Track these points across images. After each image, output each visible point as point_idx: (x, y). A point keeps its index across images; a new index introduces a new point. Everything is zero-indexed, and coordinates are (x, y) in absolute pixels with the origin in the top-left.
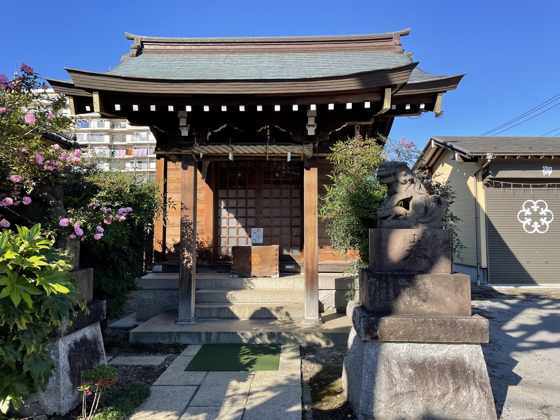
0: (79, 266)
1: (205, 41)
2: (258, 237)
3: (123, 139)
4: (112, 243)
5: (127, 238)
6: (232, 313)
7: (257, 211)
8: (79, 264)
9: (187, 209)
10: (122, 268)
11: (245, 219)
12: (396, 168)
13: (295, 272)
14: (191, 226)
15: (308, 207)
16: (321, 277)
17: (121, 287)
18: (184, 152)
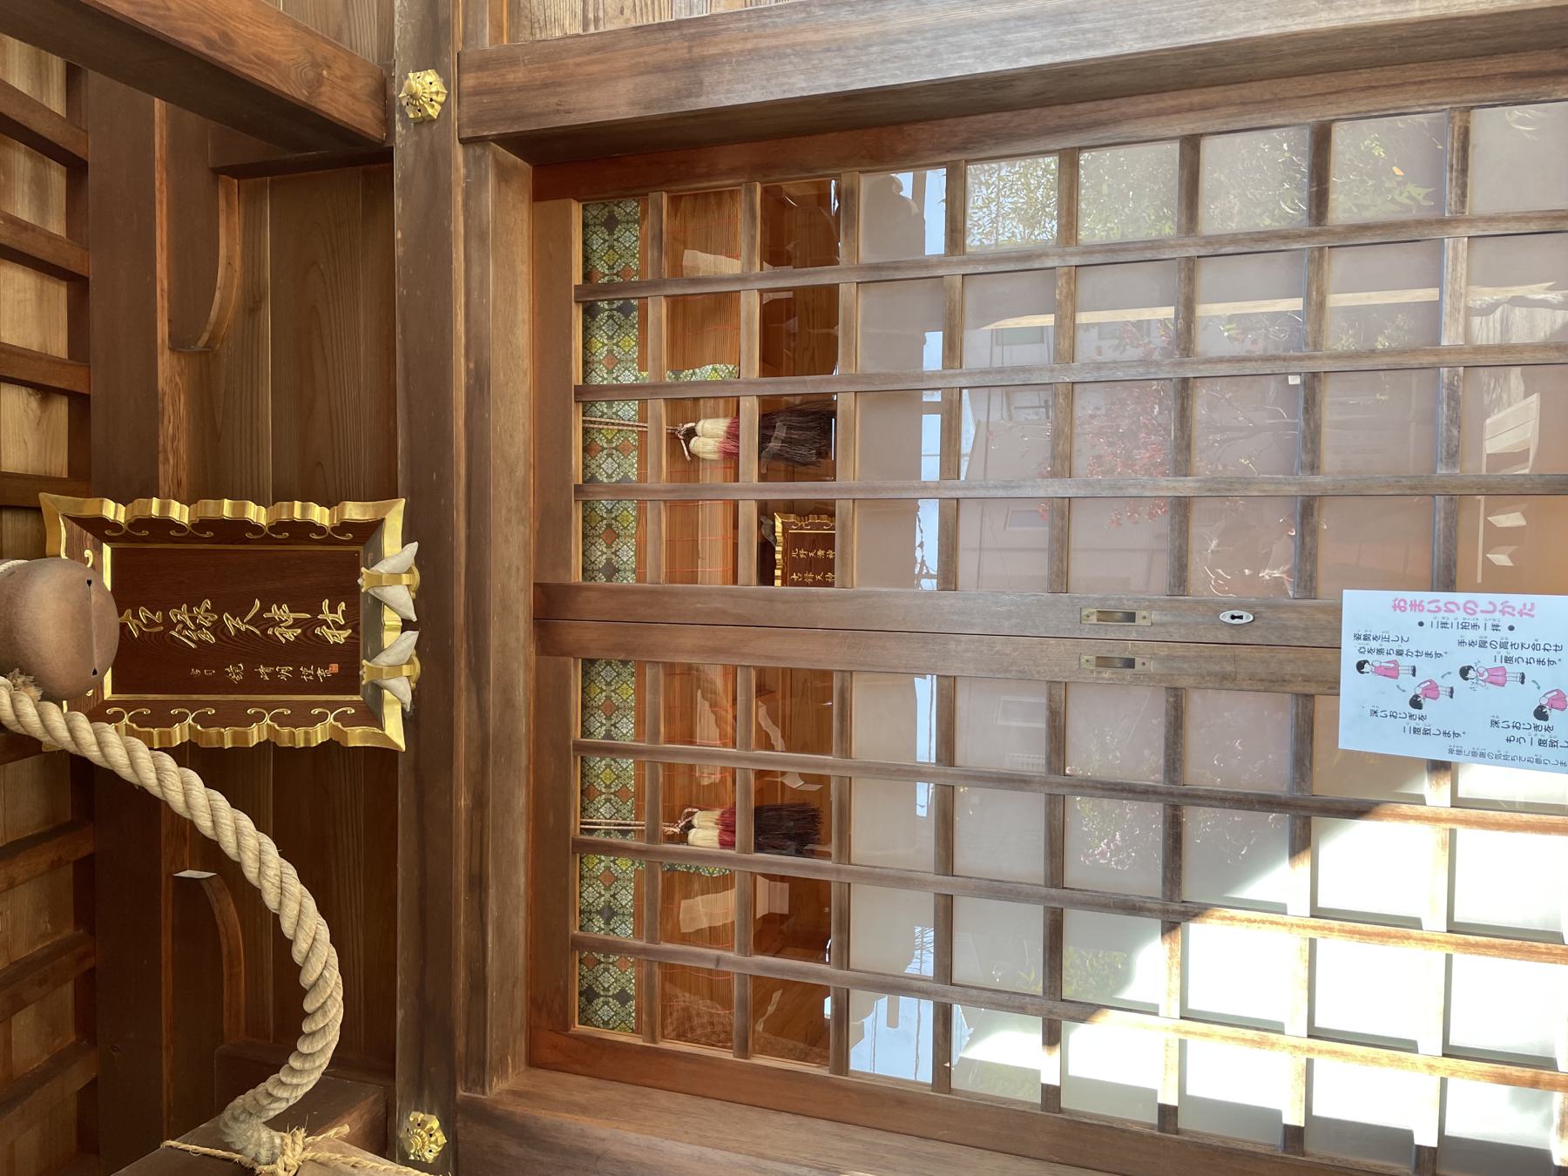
2: (1485, 659)
7: (1103, 662)
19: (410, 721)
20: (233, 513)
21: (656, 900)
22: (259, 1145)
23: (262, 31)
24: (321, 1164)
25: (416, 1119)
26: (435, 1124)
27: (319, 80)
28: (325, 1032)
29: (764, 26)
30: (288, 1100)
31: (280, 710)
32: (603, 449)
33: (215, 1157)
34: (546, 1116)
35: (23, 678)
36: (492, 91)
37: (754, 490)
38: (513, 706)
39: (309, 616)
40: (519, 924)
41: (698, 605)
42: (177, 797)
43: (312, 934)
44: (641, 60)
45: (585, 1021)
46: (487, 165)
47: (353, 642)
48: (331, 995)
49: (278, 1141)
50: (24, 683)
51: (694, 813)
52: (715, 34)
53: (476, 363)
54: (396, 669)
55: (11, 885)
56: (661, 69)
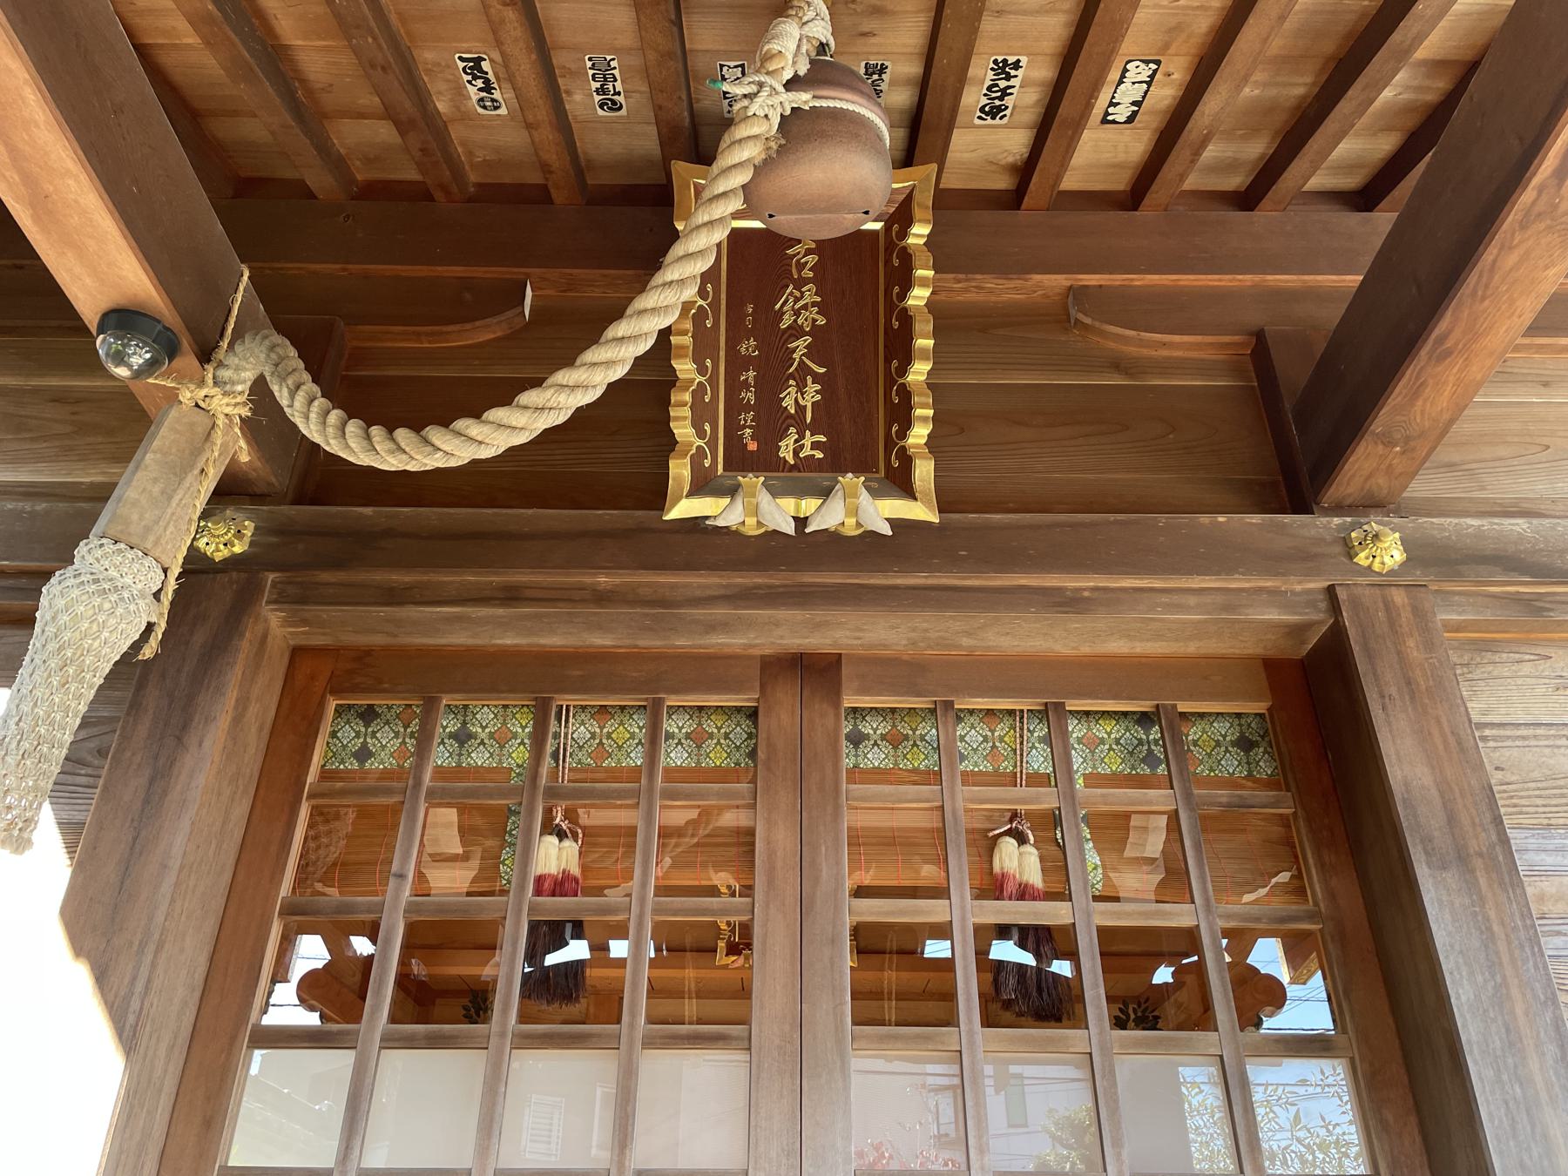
19: (695, 525)
20: (920, 349)
21: (478, 798)
22: (237, 369)
23: (1449, 388)
24: (209, 433)
25: (246, 528)
26: (238, 549)
27: (1391, 444)
28: (369, 451)
29: (1522, 947)
30: (291, 406)
31: (709, 392)
32: (993, 731)
33: (227, 320)
34: (234, 676)
35: (775, 147)
36: (1392, 622)
37: (963, 919)
38: (707, 633)
39: (808, 421)
40: (459, 638)
41: (823, 849)
42: (651, 301)
43: (487, 441)
44: (1457, 795)
45: (339, 711)
46: (1306, 614)
47: (782, 465)
48: (412, 458)
49: (239, 388)
50: (769, 149)
51: (576, 841)
52: (1501, 883)
53: (1088, 598)
54: (755, 511)
55: (529, 126)
56: (1452, 819)
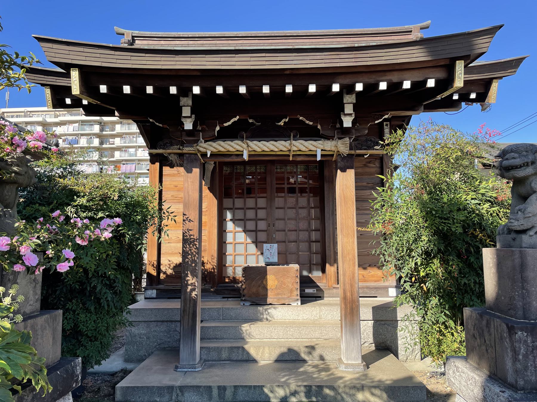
0: (39, 309)
1: (203, 36)
2: (272, 254)
3: (112, 156)
4: (94, 267)
5: (114, 260)
6: (248, 353)
7: (269, 224)
8: (39, 306)
9: (190, 220)
10: (107, 300)
11: (254, 233)
12: (534, 154)
13: (317, 297)
14: (196, 243)
15: (344, 217)
16: (364, 305)
17: (106, 325)
18: (187, 150)
